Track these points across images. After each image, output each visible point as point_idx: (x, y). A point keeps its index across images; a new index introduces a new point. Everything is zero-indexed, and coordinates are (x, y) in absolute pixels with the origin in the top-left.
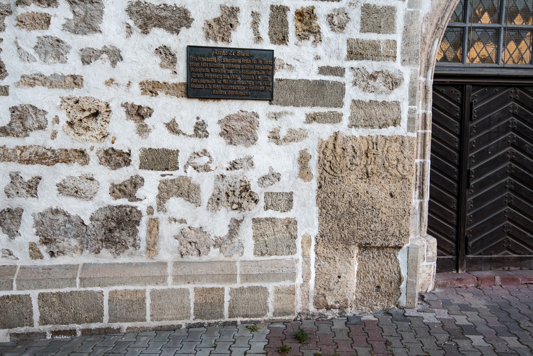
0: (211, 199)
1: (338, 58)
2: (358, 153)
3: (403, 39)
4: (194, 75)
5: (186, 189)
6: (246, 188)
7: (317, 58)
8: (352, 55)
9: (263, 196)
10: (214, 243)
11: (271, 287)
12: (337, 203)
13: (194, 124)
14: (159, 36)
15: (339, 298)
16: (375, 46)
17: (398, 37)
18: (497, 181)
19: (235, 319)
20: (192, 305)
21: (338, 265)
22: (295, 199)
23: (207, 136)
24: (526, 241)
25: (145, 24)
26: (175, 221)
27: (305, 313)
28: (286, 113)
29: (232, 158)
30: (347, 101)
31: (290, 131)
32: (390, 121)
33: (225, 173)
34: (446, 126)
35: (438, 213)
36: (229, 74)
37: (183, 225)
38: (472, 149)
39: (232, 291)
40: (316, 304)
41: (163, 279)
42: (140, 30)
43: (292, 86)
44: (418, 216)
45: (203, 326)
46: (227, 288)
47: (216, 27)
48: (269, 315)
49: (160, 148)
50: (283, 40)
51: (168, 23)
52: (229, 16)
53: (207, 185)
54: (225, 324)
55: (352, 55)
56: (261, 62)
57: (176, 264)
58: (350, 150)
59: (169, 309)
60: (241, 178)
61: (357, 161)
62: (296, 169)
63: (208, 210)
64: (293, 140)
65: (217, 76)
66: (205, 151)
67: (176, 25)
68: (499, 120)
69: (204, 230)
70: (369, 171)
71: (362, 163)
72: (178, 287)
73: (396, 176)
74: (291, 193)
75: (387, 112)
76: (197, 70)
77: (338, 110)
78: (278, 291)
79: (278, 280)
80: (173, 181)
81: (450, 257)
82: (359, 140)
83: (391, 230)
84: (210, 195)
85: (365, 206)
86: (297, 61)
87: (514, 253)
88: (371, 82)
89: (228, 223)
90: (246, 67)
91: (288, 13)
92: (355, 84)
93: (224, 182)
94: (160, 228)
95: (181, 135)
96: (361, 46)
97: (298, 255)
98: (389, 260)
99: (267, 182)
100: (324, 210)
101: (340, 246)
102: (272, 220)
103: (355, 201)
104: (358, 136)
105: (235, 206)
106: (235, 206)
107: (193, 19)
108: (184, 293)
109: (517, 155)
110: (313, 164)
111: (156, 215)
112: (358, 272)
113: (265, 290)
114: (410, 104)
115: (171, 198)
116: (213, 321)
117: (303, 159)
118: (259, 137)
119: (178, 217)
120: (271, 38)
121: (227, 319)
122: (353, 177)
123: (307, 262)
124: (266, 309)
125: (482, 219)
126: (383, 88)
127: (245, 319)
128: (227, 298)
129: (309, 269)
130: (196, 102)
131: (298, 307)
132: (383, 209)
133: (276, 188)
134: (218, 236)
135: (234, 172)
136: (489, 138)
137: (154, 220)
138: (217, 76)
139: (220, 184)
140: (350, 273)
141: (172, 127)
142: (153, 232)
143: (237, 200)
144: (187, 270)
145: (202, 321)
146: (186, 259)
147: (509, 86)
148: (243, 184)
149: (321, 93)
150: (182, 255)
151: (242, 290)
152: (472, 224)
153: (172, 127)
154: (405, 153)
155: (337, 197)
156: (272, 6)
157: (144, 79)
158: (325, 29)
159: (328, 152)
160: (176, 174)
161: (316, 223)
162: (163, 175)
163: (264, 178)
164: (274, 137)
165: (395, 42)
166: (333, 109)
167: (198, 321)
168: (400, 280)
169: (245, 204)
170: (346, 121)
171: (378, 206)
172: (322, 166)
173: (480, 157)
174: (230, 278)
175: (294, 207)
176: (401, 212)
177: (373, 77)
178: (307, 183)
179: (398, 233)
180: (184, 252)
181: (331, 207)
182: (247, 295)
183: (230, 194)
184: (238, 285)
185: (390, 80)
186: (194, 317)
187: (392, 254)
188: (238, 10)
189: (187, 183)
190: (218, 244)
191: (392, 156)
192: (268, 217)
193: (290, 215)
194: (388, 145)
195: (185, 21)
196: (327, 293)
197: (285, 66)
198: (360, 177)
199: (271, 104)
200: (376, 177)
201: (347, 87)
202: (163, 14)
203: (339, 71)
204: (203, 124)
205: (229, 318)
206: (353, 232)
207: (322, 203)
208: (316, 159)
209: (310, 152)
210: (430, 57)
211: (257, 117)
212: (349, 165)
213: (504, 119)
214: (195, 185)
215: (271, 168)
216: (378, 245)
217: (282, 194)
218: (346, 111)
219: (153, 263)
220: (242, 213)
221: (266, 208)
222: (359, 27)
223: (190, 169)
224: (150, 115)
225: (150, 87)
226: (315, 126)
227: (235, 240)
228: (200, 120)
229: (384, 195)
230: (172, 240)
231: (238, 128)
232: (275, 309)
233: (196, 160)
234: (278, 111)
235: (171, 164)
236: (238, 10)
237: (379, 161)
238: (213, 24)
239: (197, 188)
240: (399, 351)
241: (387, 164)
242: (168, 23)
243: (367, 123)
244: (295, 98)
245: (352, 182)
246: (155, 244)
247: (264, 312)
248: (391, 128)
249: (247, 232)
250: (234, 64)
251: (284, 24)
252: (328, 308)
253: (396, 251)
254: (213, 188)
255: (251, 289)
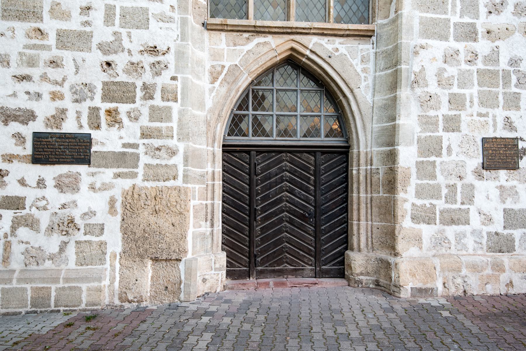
0: (47, 228)
1: (135, 138)
2: (149, 198)
3: (178, 126)
4: (36, 150)
5: (30, 222)
6: (72, 221)
7: (121, 138)
8: (144, 135)
9: (83, 226)
10: (49, 257)
11: (84, 286)
12: (134, 230)
13: (37, 180)
14: (15, 127)
15: (136, 295)
16: (159, 130)
17: (174, 124)
18: (277, 215)
19: (59, 308)
20: (29, 299)
21: (135, 272)
22: (105, 228)
23: (45, 188)
24: (299, 257)
25: (6, 120)
26: (23, 242)
27: (111, 305)
28: (100, 172)
29: (63, 201)
30: (141, 164)
31: (103, 184)
32: (171, 177)
33: (57, 211)
34: (240, 178)
35: (236, 238)
36: (60, 149)
37: (28, 246)
38: (258, 194)
39: (57, 290)
40: (120, 298)
41: (10, 281)
42: (3, 124)
43: (104, 155)
44: (210, 240)
45: (37, 313)
46: (53, 287)
47: (52, 120)
48: (83, 306)
49: (14, 195)
50: (98, 127)
51: (21, 119)
52: (61, 114)
53: (45, 219)
54: (52, 311)
55: (144, 135)
56: (82, 141)
57: (22, 271)
58: (143, 195)
59: (13, 301)
60: (68, 214)
61: (149, 202)
62: (107, 207)
63: (45, 235)
64: (105, 189)
65: (52, 150)
66: (44, 197)
67: (26, 120)
68: (277, 175)
69: (42, 249)
70: (157, 209)
71: (152, 204)
72: (20, 286)
73: (175, 212)
74: (103, 224)
75: (168, 171)
76: (38, 147)
77: (135, 170)
78: (89, 289)
79: (89, 282)
80: (22, 216)
81: (245, 268)
82: (150, 189)
83: (173, 248)
84: (47, 226)
85: (154, 232)
86: (106, 140)
87: (292, 266)
88: (157, 152)
89: (59, 244)
90: (71, 144)
91: (100, 111)
92: (146, 154)
93: (57, 217)
94: (12, 247)
95: (28, 187)
96: (149, 130)
97: (107, 265)
98: (174, 269)
99: (87, 217)
100: (125, 235)
101: (137, 259)
102: (89, 242)
103: (148, 229)
104: (149, 187)
105: (64, 233)
106: (64, 233)
107: (37, 116)
108: (24, 290)
109: (290, 197)
110: (118, 206)
111: (9, 238)
112: (152, 277)
113: (80, 288)
114: (184, 166)
115: (20, 228)
116: (43, 309)
117: (112, 202)
118: (81, 188)
119: (25, 240)
120: (90, 126)
121: (53, 308)
122: (146, 213)
123: (113, 270)
124: (81, 302)
125: (268, 242)
126: (165, 156)
127: (66, 308)
128: (53, 294)
129: (115, 275)
130: (38, 167)
131: (107, 301)
132: (167, 234)
133: (93, 221)
134: (51, 252)
135: (64, 211)
136: (270, 186)
137: (9, 242)
138: (52, 150)
139: (53, 218)
140: (146, 279)
141: (22, 182)
142: (7, 250)
143: (65, 229)
144: (27, 275)
145: (36, 310)
146: (28, 268)
147: (281, 152)
148: (70, 218)
149: (123, 160)
150: (26, 265)
151: (63, 289)
152: (260, 245)
153: (22, 182)
154: (181, 197)
155: (135, 227)
156: (89, 107)
157: (4, 153)
158: (125, 120)
159: (129, 197)
160: (24, 212)
161: (120, 244)
162: (15, 213)
163: (85, 214)
164: (92, 188)
165: (172, 127)
166: (131, 170)
167: (33, 309)
168: (181, 282)
169: (70, 231)
170: (140, 177)
171: (163, 233)
172: (125, 207)
173: (264, 199)
174: (56, 280)
175: (105, 233)
176: (180, 236)
177: (158, 149)
178: (114, 217)
179: (178, 250)
180: (27, 263)
181: (131, 233)
182: (68, 292)
183: (61, 225)
184: (61, 285)
185: (170, 151)
186: (30, 307)
187: (176, 265)
188: (67, 110)
189: (31, 218)
190: (51, 258)
191: (172, 200)
192: (87, 240)
193: (102, 238)
194: (170, 192)
195: (32, 118)
196: (128, 292)
197: (99, 143)
198: (151, 213)
199: (89, 167)
200: (162, 213)
201: (141, 156)
202: (18, 113)
203: (135, 146)
204: (43, 180)
205: (55, 307)
206: (146, 250)
207: (127, 231)
208: (121, 202)
209: (116, 197)
210: (216, 134)
211: (80, 175)
212: (143, 205)
213: (280, 173)
214: (37, 219)
215: (89, 208)
216: (164, 258)
217: (97, 225)
218: (140, 170)
219: (7, 271)
220: (69, 237)
221: (85, 234)
222: (148, 119)
223: (34, 209)
224: (7, 175)
225: (8, 158)
226: (119, 180)
227: (63, 255)
228: (41, 178)
229: (167, 225)
230: (20, 255)
231: (67, 182)
232: (87, 302)
233: (38, 203)
234: (94, 171)
235: (21, 205)
236: (67, 110)
237: (164, 202)
238: (51, 119)
239: (38, 221)
240: (280, 346)
241: (169, 205)
242: (21, 119)
243: (155, 178)
244: (106, 163)
245: (146, 217)
246: (8, 258)
247: (79, 304)
248: (172, 181)
249: (71, 251)
250: (64, 142)
251: (98, 117)
252: (130, 302)
253: (178, 263)
254: (49, 221)
255: (70, 288)
